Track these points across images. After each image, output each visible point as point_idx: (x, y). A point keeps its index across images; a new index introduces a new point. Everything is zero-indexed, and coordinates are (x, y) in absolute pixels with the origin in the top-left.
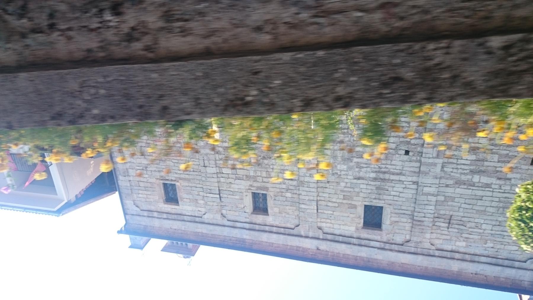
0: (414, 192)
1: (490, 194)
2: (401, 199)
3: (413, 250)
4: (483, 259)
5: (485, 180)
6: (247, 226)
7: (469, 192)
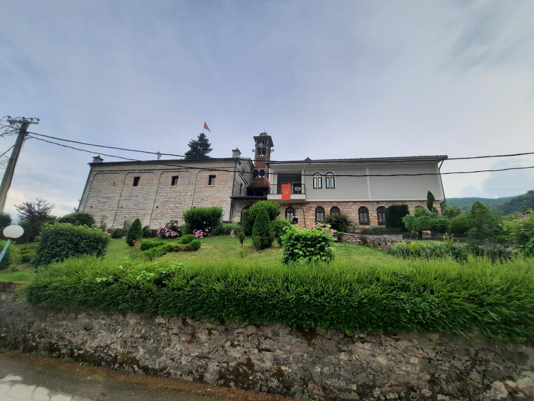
2: (126, 190)
3: (126, 171)
4: (107, 172)
5: (103, 200)
7: (108, 195)
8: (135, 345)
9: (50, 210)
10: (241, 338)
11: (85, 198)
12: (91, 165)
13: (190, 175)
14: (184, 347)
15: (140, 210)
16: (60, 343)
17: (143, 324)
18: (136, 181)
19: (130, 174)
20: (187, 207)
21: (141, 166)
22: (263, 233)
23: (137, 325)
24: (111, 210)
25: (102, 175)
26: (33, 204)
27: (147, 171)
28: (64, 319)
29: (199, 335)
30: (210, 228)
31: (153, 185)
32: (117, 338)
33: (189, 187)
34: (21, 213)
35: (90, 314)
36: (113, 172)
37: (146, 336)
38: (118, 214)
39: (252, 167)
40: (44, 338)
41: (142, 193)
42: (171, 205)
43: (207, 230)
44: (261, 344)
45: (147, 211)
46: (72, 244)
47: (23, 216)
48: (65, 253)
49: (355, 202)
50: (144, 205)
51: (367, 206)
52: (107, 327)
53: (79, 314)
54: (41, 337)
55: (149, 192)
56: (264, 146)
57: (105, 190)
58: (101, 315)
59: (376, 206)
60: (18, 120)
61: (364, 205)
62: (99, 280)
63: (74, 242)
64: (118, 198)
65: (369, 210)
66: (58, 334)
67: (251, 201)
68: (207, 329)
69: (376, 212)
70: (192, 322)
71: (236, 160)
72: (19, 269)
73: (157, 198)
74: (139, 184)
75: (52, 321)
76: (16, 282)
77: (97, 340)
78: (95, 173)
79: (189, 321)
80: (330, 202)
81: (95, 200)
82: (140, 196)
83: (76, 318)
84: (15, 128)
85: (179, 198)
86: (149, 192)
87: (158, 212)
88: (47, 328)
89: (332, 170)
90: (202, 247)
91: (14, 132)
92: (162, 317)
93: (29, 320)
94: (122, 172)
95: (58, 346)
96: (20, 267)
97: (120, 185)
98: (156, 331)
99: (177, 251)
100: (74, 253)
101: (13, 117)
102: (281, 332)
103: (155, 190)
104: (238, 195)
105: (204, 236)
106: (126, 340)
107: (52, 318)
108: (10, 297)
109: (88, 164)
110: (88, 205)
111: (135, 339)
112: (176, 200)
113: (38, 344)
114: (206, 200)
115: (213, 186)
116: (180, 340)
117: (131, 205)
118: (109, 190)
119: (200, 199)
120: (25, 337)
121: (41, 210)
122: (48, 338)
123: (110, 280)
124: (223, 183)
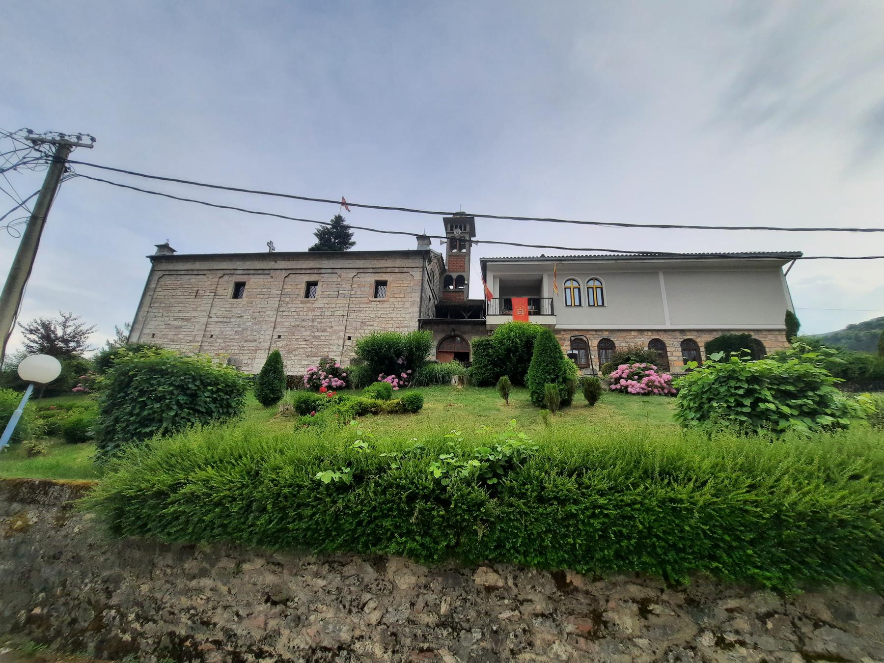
0: (212, 311)
1: (175, 315)
4: (183, 273)
5: (176, 323)
6: (323, 271)
8: (426, 646)
9: (85, 335)
10: (742, 623)
11: (140, 318)
12: (153, 259)
13: (339, 280)
14: (577, 649)
15: (246, 341)
16: (200, 637)
17: (440, 588)
18: (239, 289)
19: (226, 278)
20: (364, 334)
21: (248, 263)
22: (557, 377)
23: (422, 591)
24: (190, 341)
25: (173, 278)
26: (54, 322)
27: (260, 272)
28: (204, 573)
29: (609, 616)
30: (409, 371)
31: (271, 296)
32: (369, 625)
33: (338, 302)
34: (29, 339)
35: (276, 562)
36: (195, 272)
37: (457, 620)
38: (205, 348)
39: (443, 270)
40: (155, 622)
41: (251, 311)
42: (304, 334)
43: (404, 375)
44: (807, 641)
45: (260, 343)
46: (186, 394)
47: (32, 347)
48: (172, 413)
49: (641, 331)
50: (255, 333)
51: (663, 337)
52: (334, 597)
53: (244, 561)
54: (144, 619)
55: (265, 310)
56: (462, 235)
57: (180, 305)
58: (309, 564)
59: (681, 338)
60: (50, 138)
61: (657, 337)
62: (325, 477)
63: (188, 392)
64: (204, 320)
65: (667, 345)
66: (192, 612)
67: (453, 326)
68: (634, 601)
69: (680, 349)
70: (585, 584)
71: (424, 255)
72: (43, 449)
73: (278, 320)
74: (245, 294)
75: (171, 578)
76: (62, 481)
77: (312, 631)
78: (161, 273)
79: (574, 579)
80: (596, 331)
81: (160, 323)
82: (246, 316)
83: (238, 572)
84: (45, 153)
85: (319, 320)
86: (265, 310)
87: (280, 345)
88: (158, 596)
89: (596, 274)
90: (424, 406)
91: (42, 161)
92: (491, 570)
93: (106, 573)
94: (212, 272)
95: (195, 645)
96: (43, 445)
97: (208, 297)
98: (483, 607)
99: (375, 413)
100: (189, 414)
101: (40, 130)
102: (858, 609)
103: (273, 306)
104: (426, 317)
105: (400, 386)
106: (394, 630)
107: (169, 571)
108: (51, 515)
109: (147, 257)
110: (146, 331)
111: (424, 628)
112: (315, 324)
113: (136, 635)
114: (371, 325)
115: (384, 299)
116: (560, 633)
117: (228, 331)
118: (188, 305)
119: (359, 323)
120: (99, 618)
121: (69, 335)
122: (165, 621)
123: (345, 478)
124: (403, 295)
